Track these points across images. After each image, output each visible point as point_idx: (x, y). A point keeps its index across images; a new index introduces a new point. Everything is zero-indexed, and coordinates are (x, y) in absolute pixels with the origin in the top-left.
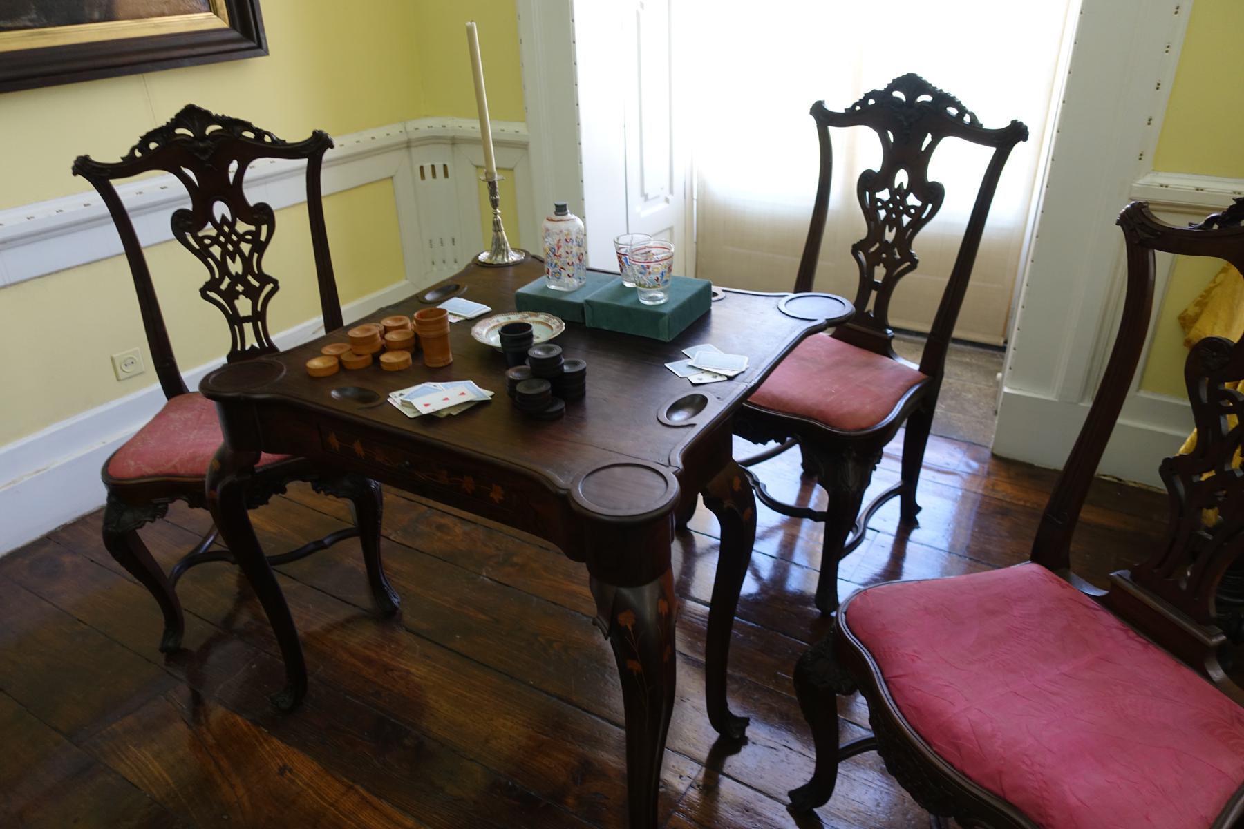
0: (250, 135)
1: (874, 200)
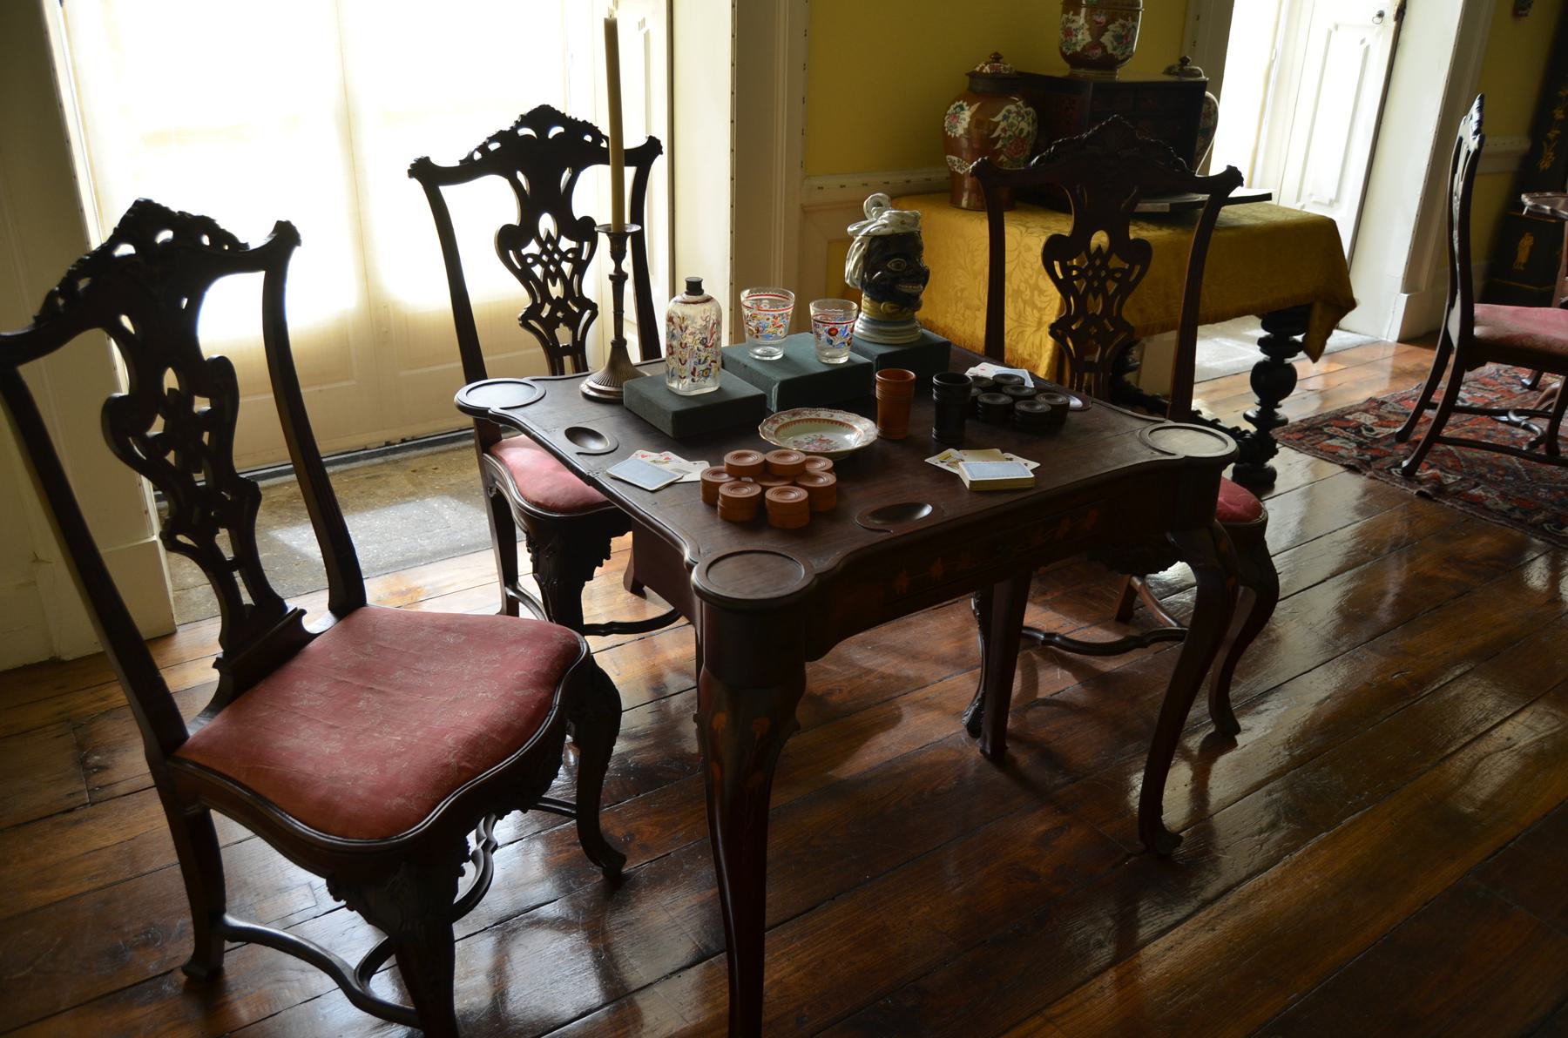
0: (588, 138)
1: (522, 259)
